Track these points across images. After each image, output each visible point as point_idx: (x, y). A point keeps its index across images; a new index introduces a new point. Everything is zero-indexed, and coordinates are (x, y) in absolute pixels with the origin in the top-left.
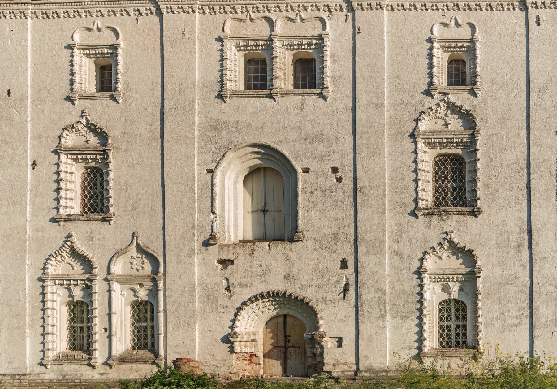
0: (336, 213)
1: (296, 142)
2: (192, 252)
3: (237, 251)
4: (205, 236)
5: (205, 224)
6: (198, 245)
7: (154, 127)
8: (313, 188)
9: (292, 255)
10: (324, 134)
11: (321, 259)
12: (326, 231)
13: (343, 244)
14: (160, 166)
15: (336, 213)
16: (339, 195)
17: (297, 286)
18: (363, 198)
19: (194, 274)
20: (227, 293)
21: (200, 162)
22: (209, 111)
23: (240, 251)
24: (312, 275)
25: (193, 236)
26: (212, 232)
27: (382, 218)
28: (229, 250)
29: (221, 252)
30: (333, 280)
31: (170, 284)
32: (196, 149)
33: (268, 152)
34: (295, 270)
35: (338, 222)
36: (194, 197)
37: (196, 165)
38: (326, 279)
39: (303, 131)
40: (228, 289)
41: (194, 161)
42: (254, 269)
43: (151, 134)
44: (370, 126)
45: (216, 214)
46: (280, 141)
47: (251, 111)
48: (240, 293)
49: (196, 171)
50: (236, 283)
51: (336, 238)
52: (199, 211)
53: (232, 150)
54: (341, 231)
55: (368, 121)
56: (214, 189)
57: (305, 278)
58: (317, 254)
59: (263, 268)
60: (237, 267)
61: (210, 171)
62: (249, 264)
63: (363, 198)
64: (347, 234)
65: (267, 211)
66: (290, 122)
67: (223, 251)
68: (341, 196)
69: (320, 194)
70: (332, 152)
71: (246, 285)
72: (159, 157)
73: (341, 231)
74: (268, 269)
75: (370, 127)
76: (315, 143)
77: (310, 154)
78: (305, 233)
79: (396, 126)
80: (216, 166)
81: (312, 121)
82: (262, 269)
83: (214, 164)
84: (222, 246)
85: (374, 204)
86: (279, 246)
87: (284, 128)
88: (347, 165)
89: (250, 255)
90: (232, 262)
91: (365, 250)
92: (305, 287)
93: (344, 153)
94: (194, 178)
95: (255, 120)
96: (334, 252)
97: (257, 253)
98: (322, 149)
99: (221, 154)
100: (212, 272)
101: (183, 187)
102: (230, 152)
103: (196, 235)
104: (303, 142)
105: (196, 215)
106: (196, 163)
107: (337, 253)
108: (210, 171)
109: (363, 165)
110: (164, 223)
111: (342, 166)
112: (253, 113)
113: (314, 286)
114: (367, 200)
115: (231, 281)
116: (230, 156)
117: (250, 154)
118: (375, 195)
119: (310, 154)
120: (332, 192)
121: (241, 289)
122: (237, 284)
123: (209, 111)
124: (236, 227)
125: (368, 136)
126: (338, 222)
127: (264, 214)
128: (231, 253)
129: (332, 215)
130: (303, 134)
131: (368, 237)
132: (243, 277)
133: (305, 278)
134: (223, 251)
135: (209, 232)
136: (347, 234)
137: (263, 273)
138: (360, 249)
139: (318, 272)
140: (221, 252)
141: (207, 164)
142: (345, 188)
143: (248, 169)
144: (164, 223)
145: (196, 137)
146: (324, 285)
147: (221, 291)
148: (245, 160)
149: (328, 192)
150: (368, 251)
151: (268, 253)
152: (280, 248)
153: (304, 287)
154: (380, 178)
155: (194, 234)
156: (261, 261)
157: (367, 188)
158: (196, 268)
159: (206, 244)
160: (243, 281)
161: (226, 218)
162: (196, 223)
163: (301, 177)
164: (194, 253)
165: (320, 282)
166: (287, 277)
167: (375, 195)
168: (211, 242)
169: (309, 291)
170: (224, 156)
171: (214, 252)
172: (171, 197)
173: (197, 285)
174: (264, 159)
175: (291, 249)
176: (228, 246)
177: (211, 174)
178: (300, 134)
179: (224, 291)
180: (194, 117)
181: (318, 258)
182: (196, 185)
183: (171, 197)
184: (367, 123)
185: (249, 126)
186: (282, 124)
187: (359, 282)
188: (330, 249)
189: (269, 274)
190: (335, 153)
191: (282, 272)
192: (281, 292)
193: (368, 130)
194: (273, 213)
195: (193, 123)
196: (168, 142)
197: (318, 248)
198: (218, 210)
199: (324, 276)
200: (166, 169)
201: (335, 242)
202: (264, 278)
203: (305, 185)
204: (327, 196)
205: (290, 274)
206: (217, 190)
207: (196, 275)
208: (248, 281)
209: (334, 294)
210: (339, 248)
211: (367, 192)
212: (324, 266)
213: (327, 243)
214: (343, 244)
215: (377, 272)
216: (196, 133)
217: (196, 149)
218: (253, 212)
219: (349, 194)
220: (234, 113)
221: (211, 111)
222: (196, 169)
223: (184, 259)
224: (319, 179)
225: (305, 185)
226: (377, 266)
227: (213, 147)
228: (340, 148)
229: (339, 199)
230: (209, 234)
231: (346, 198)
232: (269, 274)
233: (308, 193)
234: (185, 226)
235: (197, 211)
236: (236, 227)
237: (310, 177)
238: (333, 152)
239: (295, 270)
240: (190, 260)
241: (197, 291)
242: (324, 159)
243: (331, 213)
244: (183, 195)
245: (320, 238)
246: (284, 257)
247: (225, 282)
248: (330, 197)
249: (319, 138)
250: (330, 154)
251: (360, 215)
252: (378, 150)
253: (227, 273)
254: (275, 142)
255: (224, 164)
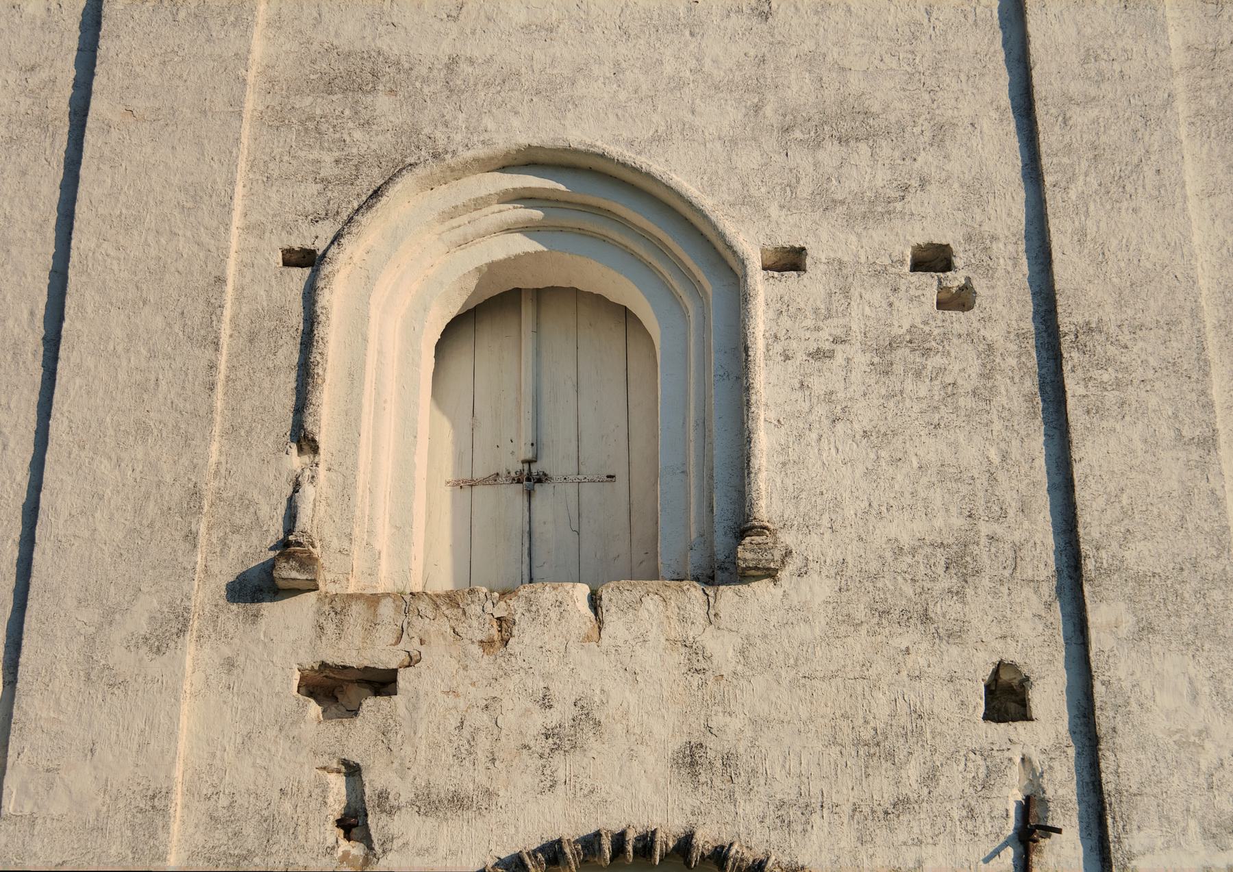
0: (955, 446)
1: (734, 142)
2: (175, 626)
3: (418, 623)
4: (255, 548)
5: (255, 494)
6: (205, 593)
7: (44, 74)
8: (824, 334)
9: (721, 649)
10: (876, 108)
11: (880, 666)
12: (904, 529)
13: (996, 594)
14: (51, 234)
15: (955, 446)
16: (963, 364)
17: (749, 809)
18: (1096, 373)
19: (172, 735)
20: (345, 845)
21: (255, 217)
22: (318, 20)
23: (436, 627)
24: (835, 750)
25: (183, 546)
26: (289, 530)
27: (1203, 466)
28: (373, 624)
29: (330, 628)
30: (955, 780)
31: (24, 790)
32: (242, 165)
33: (586, 188)
34: (735, 724)
35: (964, 489)
36: (212, 366)
37: (234, 231)
38: (913, 772)
39: (770, 96)
40: (352, 823)
41: (227, 208)
42: (508, 720)
43: (25, 102)
44: (1100, 73)
45: (315, 450)
46: (657, 139)
47: (521, 18)
48: (424, 842)
49: (233, 255)
50: (402, 790)
51: (960, 562)
52: (231, 431)
53: (420, 171)
54: (985, 529)
55: (1089, 56)
56: (319, 332)
57: (793, 763)
58: (859, 644)
59: (561, 714)
60: (414, 708)
61: (305, 259)
62: (479, 694)
63: (1096, 373)
64: (1016, 549)
65: (542, 479)
66: (707, 62)
67: (340, 625)
68: (975, 368)
69: (862, 360)
70: (915, 183)
71: (458, 802)
72: (51, 193)
73: (985, 529)
74: (586, 715)
75: (1101, 78)
76: (832, 147)
77: (805, 190)
78: (788, 538)
79: (1220, 80)
80: (337, 238)
81: (811, 61)
82: (553, 718)
83: (326, 230)
84: (338, 606)
85: (1153, 401)
86: (651, 603)
87: (678, 84)
88: (994, 238)
89: (487, 644)
90: (382, 683)
91: (1128, 623)
92: (794, 814)
93: (976, 191)
94: (220, 280)
95: (538, 55)
96: (954, 635)
97: (526, 637)
98: (866, 171)
99: (365, 187)
100: (272, 733)
101: (159, 322)
102: (406, 182)
103: (202, 540)
104: (770, 143)
105: (214, 447)
106: (237, 220)
107: (971, 637)
108: (305, 259)
109: (1082, 234)
110: (36, 486)
111: (969, 239)
112: (526, 28)
113: (847, 809)
114: (1118, 385)
115: (374, 780)
116: (403, 200)
117: (496, 207)
118: (1153, 362)
119: (805, 190)
120: (927, 352)
121: (431, 822)
122: (406, 796)
123: (318, 20)
124: (402, 529)
125: (1093, 113)
126: (964, 489)
127: (530, 494)
128: (385, 635)
129: (932, 457)
130: (768, 110)
131: (1140, 559)
132: (446, 757)
133: (793, 763)
134: (340, 625)
135: (276, 530)
136: (1016, 549)
137: (557, 740)
138: (1097, 616)
139: (867, 734)
140: (330, 628)
141: (288, 228)
142: (994, 334)
143: (472, 284)
144: (36, 486)
145: (247, 115)
146: (901, 804)
147: (314, 834)
148: (470, 230)
149: (903, 352)
150: (1146, 629)
151: (588, 638)
152: (653, 617)
153: (794, 813)
154: (1172, 291)
155: (191, 538)
156: (546, 676)
157: (1113, 329)
158: (185, 708)
159: (256, 588)
160: (444, 781)
161: (362, 478)
162: (210, 487)
163: (763, 287)
164: (181, 632)
165: (882, 788)
166: (690, 760)
167: (1153, 362)
168: (288, 572)
169: (817, 835)
170: (377, 194)
171: (291, 634)
172: (90, 362)
173: (178, 798)
174: (562, 230)
175: (712, 618)
176: (373, 600)
177: (307, 271)
178: (757, 109)
179: (333, 834)
180: (246, 34)
181: (867, 664)
182: (227, 313)
183: (90, 362)
184: (1084, 62)
185: (508, 78)
186: (668, 69)
187: (1108, 787)
188: (926, 618)
189: (593, 744)
190: (933, 188)
191: (667, 734)
192: (666, 838)
193: (1093, 91)
194: (571, 489)
195: (242, 58)
196: (107, 127)
197: (860, 613)
198: (325, 421)
199: (901, 755)
200: (81, 242)
201: (955, 583)
202: (562, 766)
203: (785, 322)
204: (898, 368)
205: (710, 742)
206: (332, 335)
207: (183, 745)
208: (469, 779)
209: (961, 850)
210: (978, 609)
211: (1112, 350)
212: (902, 708)
213: (908, 590)
214: (996, 594)
215: (1204, 733)
216: (252, 102)
217: (242, 165)
218: (466, 484)
219: (1013, 362)
220: (437, 25)
221: (326, 16)
222: (234, 244)
223: (121, 658)
224: (855, 292)
225: (785, 322)
226: (1205, 702)
227: (328, 158)
228: (954, 167)
229: (966, 385)
230: (271, 540)
231: (1001, 381)
232: (593, 744)
233: (800, 356)
234: (147, 497)
235: (217, 429)
236: (402, 529)
237: (808, 288)
238: (924, 183)
239: (735, 724)
240: (155, 666)
241: (175, 827)
242: (878, 209)
243: (930, 449)
244: (152, 355)
245: (874, 566)
246: (678, 657)
247: (337, 784)
248: (918, 374)
249: (850, 125)
250: (906, 188)
251: (1087, 456)
252: (1149, 172)
253: (359, 735)
254: (631, 144)
255: (373, 231)
